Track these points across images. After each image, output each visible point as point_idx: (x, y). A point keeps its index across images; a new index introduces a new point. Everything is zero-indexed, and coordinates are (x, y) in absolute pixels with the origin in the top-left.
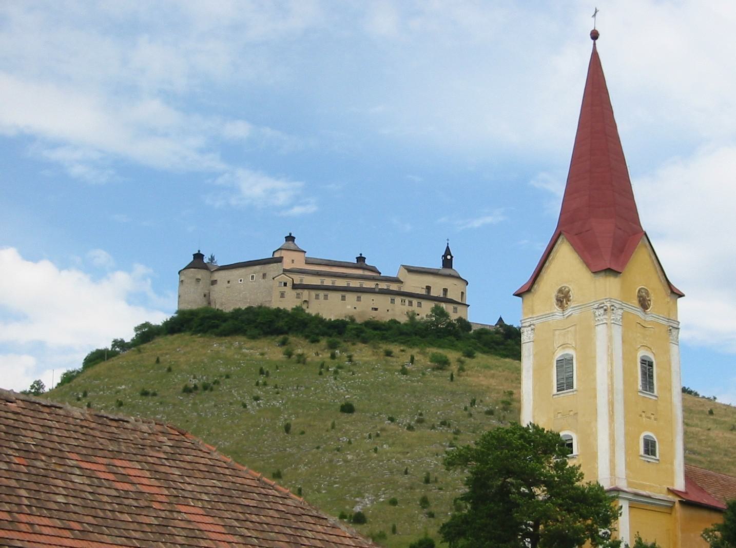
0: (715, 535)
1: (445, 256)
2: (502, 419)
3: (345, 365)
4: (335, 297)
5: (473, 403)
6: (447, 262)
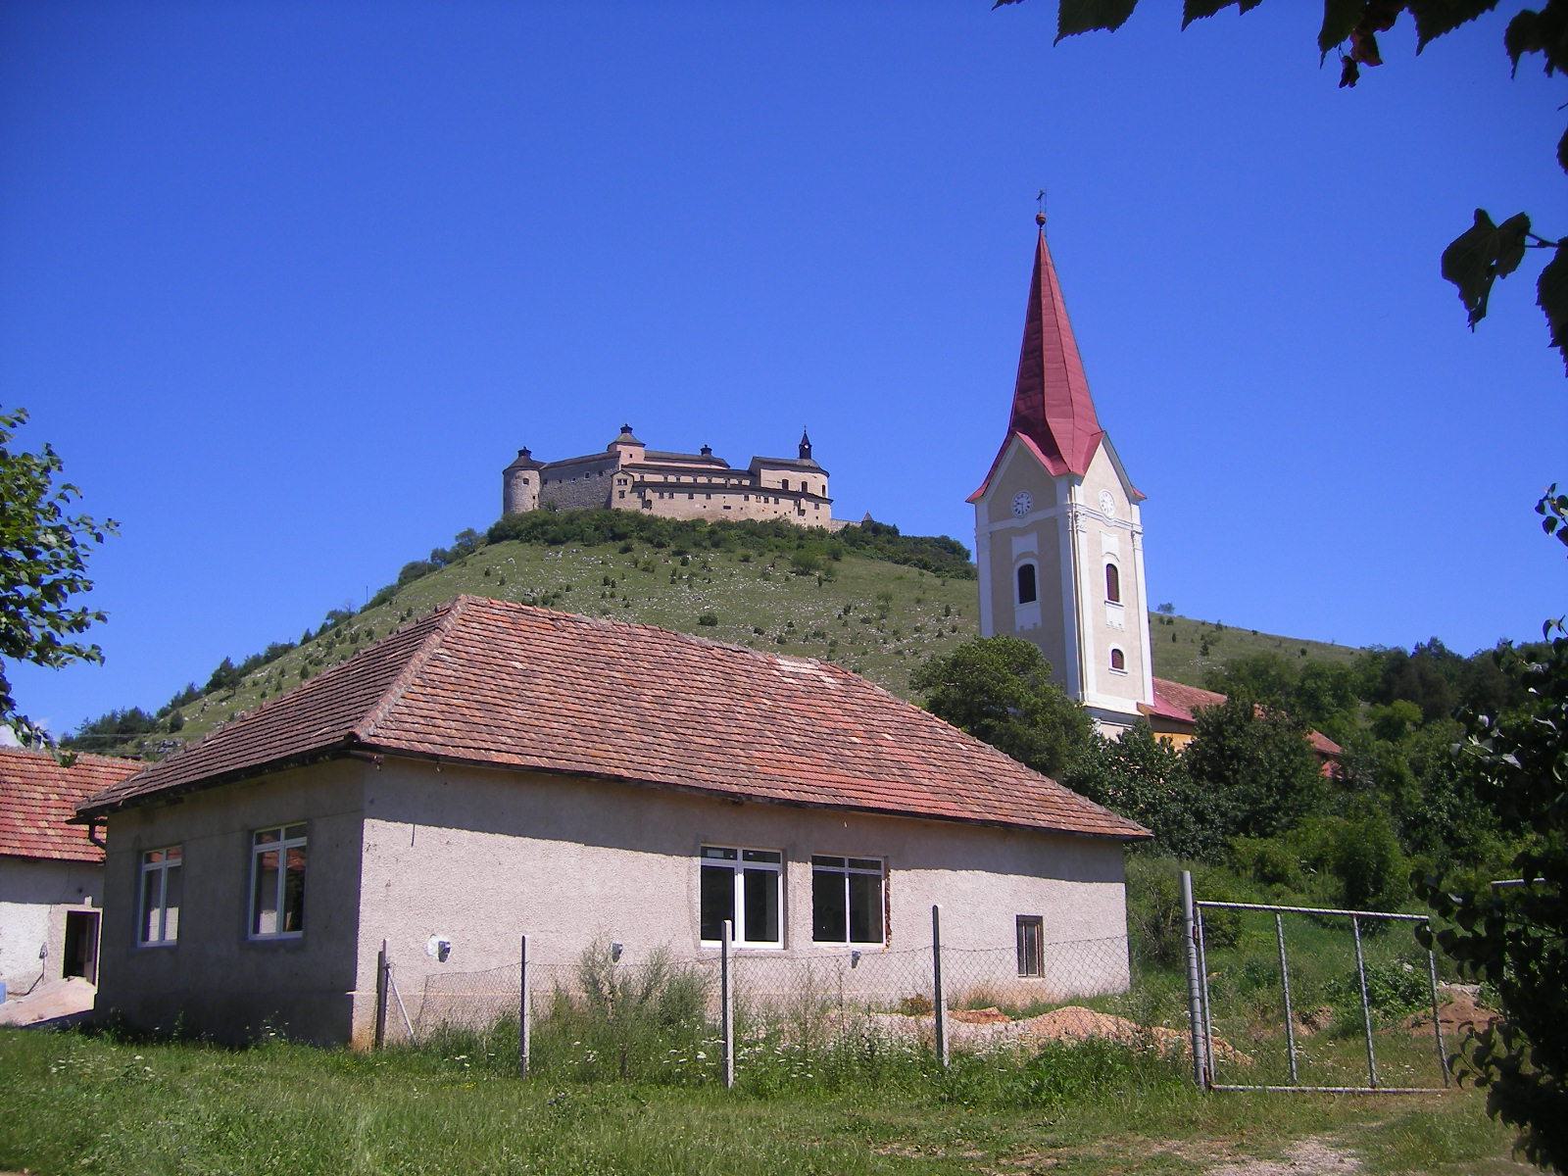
0: (1182, 820)
1: (802, 447)
2: (881, 628)
3: (142, 1051)
4: (681, 498)
5: (846, 611)
6: (805, 453)
